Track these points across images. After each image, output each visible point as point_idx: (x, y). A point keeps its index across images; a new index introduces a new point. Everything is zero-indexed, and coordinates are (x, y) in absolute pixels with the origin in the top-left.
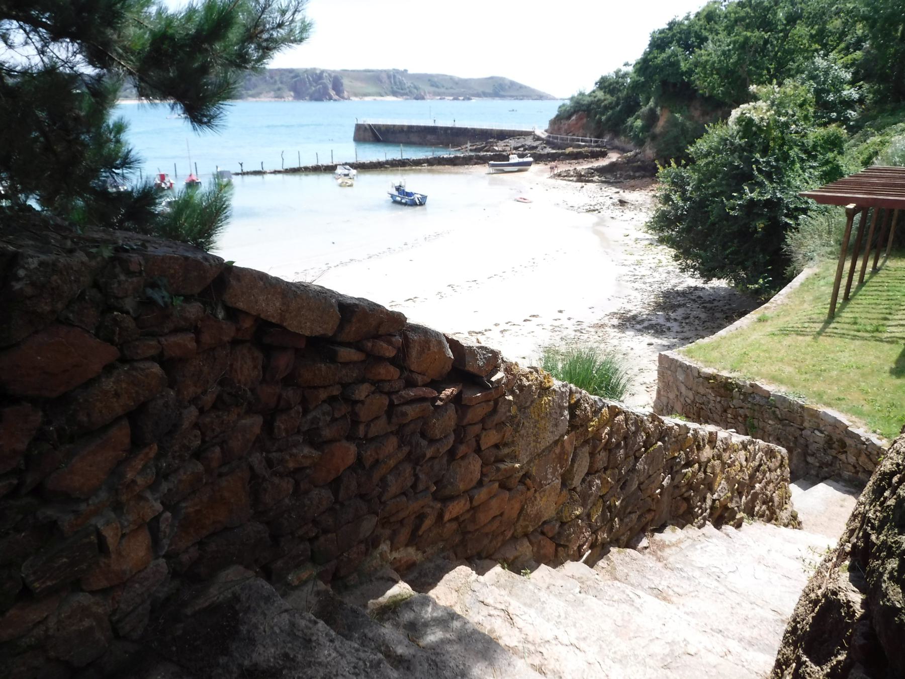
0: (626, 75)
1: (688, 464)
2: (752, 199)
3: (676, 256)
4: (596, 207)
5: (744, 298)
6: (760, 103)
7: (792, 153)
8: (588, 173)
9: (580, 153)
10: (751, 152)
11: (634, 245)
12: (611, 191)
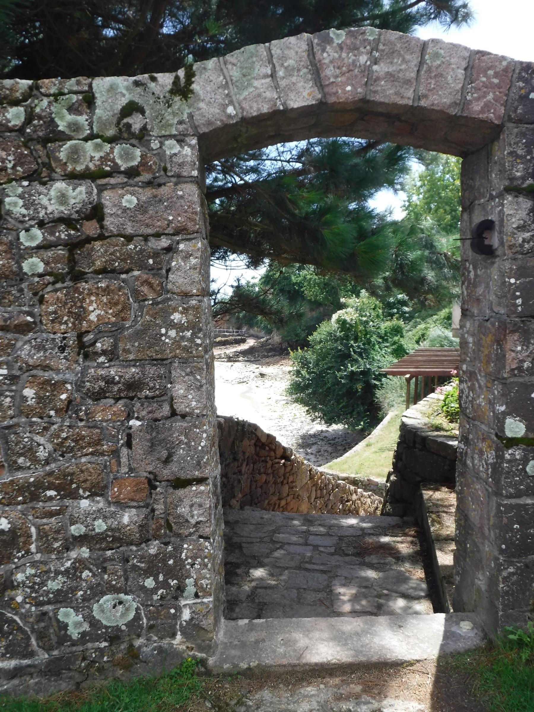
0: (254, 285)
1: (348, 501)
2: (352, 371)
3: (307, 411)
4: (245, 380)
5: (354, 435)
6: (349, 310)
7: (372, 340)
8: (235, 355)
9: (227, 340)
10: (348, 340)
11: (276, 405)
12: (253, 367)
